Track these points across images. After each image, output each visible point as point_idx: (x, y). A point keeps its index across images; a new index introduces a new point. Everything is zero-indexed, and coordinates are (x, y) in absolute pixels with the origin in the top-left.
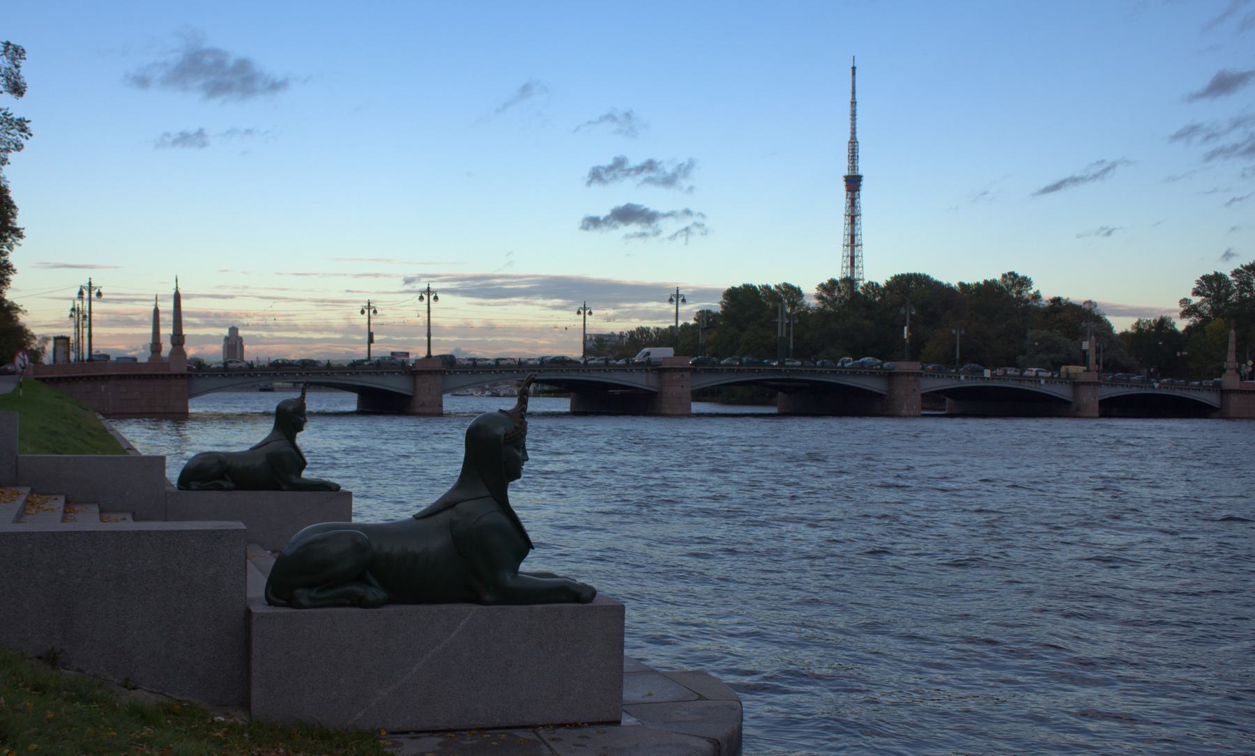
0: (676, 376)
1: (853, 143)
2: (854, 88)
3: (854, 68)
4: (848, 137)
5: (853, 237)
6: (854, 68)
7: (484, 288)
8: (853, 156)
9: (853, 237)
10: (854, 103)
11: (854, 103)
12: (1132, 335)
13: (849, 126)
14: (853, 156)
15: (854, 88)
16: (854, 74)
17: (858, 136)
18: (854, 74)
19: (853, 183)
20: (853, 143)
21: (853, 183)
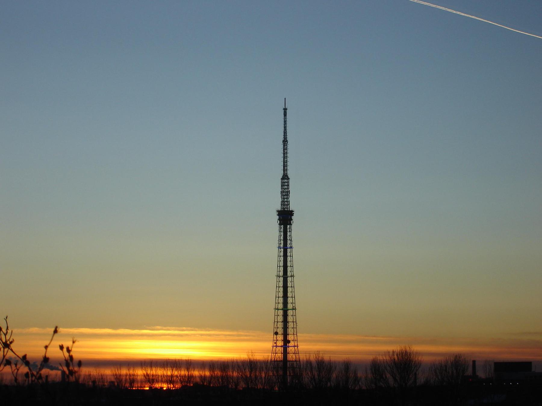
0: (290, 349)
1: (285, 177)
2: (285, 128)
3: (285, 110)
4: (282, 138)
5: (285, 256)
6: (285, 110)
7: (291, 240)
8: (285, 194)
9: (285, 256)
10: (285, 141)
11: (285, 141)
12: (281, 211)
13: (287, 128)
14: (285, 194)
15: (285, 128)
16: (285, 115)
17: (290, 174)
18: (285, 115)
19: (285, 217)
20: (285, 177)
21: (285, 217)
